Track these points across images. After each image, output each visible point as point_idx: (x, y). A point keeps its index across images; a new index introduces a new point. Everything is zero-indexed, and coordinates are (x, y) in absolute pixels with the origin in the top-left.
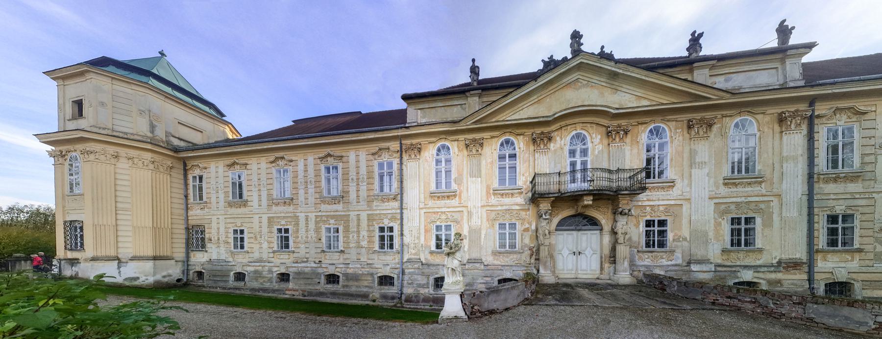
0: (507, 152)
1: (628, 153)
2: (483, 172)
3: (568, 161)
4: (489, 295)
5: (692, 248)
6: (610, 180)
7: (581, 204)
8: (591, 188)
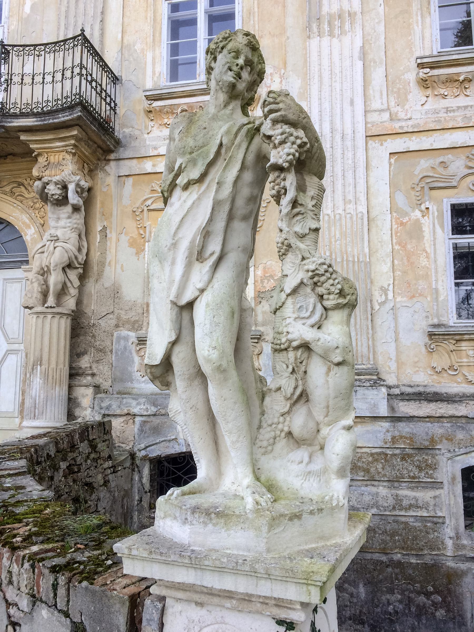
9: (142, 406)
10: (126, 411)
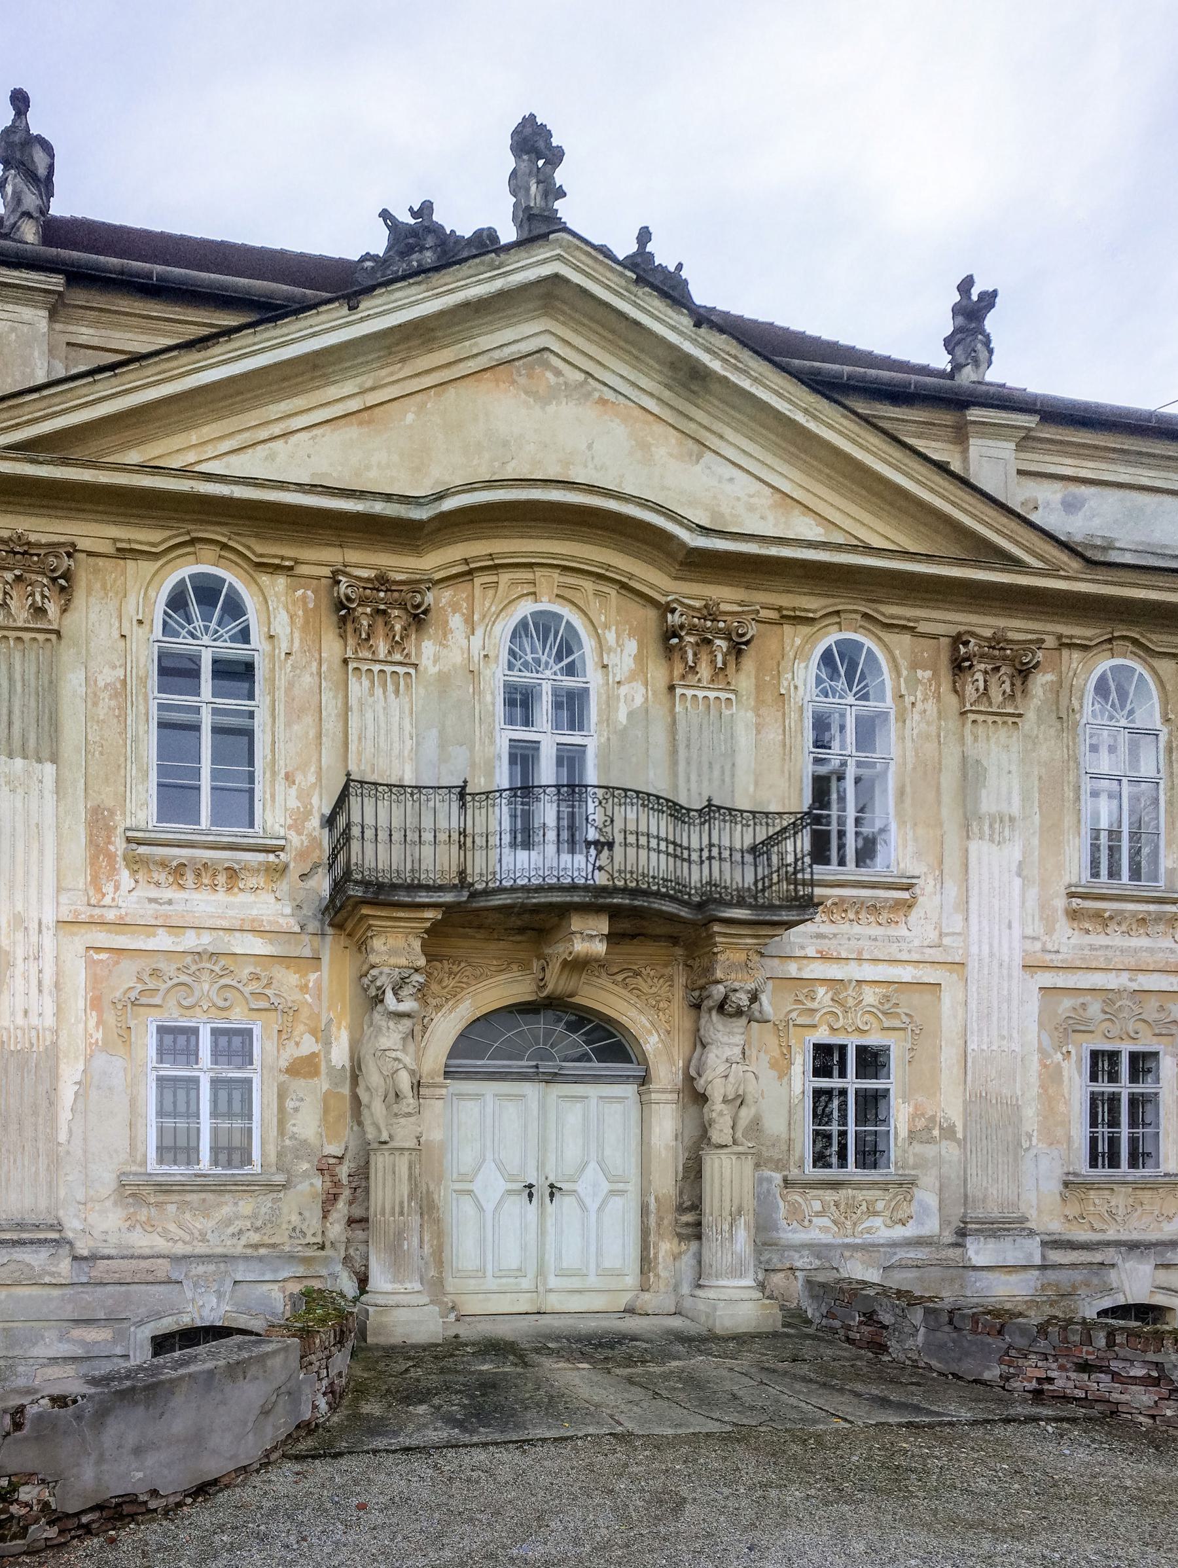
0: (208, 645)
1: (744, 739)
2: (72, 731)
3: (505, 737)
4: (102, 1414)
5: (972, 1170)
6: (678, 852)
7: (558, 951)
8: (601, 879)
9: (806, 1260)
10: (788, 1266)
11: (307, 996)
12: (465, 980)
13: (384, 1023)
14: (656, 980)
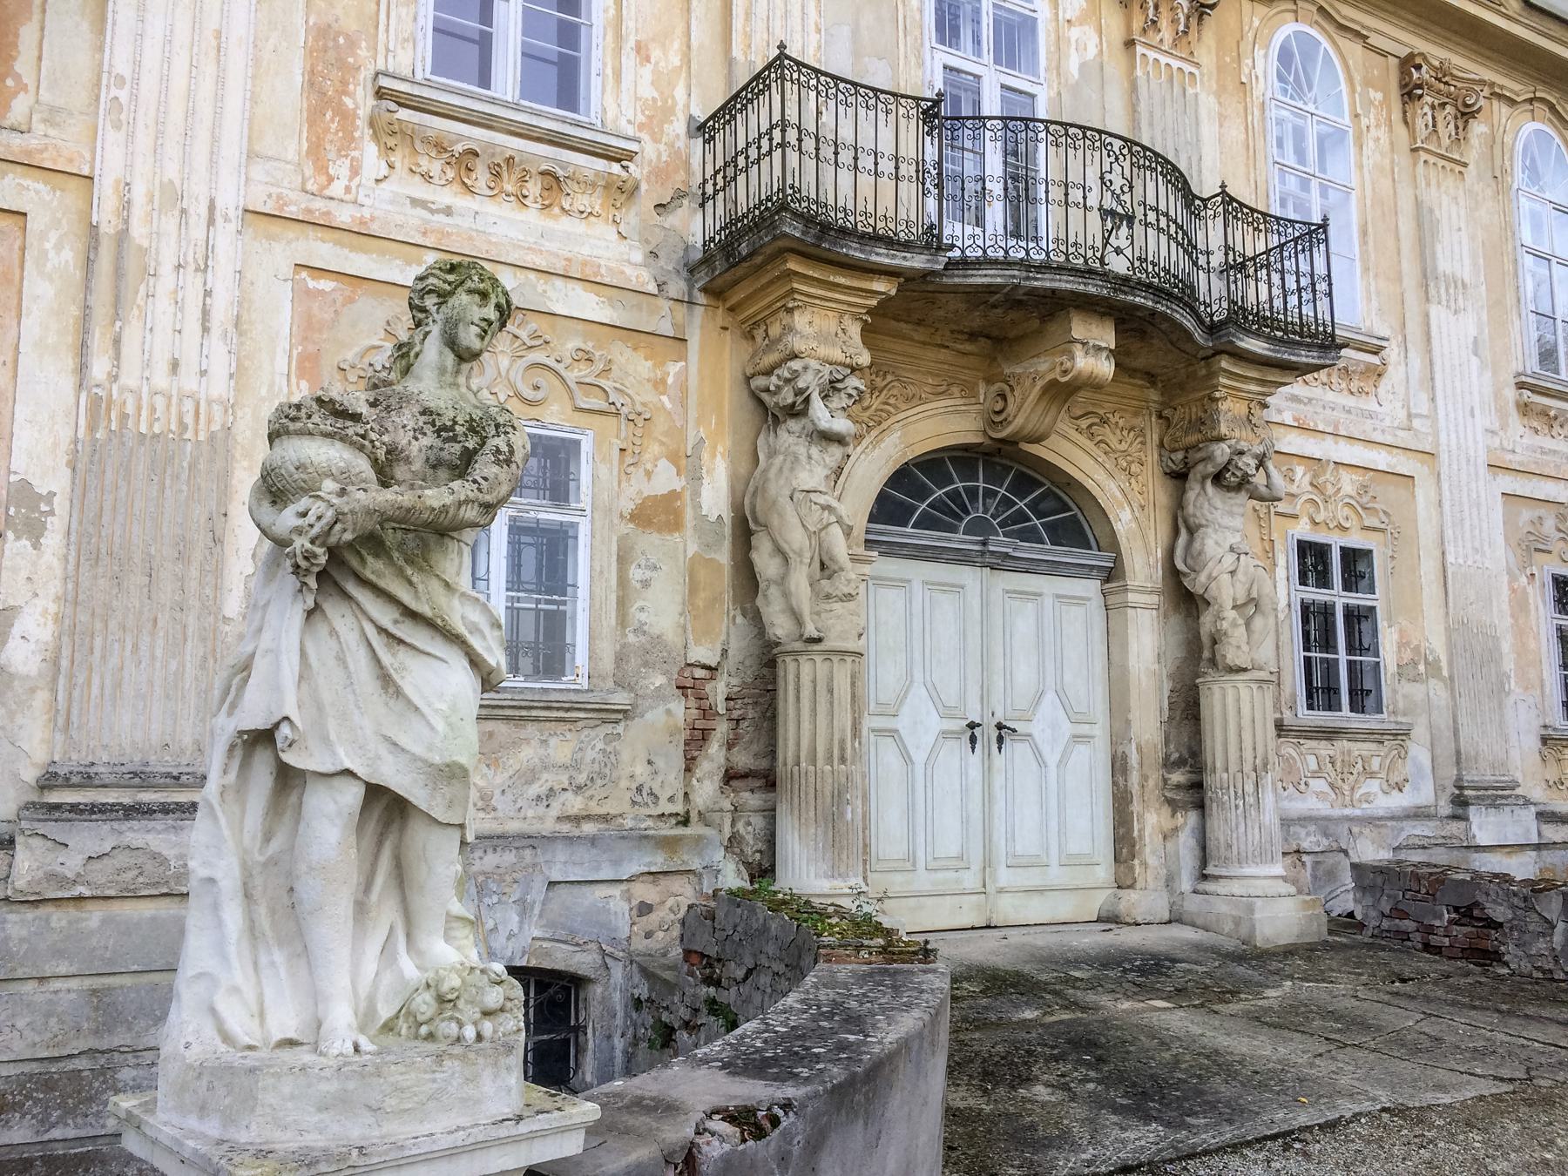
7: (1043, 367)
11: (664, 398)
12: (892, 401)
13: (802, 450)
14: (1125, 433)
